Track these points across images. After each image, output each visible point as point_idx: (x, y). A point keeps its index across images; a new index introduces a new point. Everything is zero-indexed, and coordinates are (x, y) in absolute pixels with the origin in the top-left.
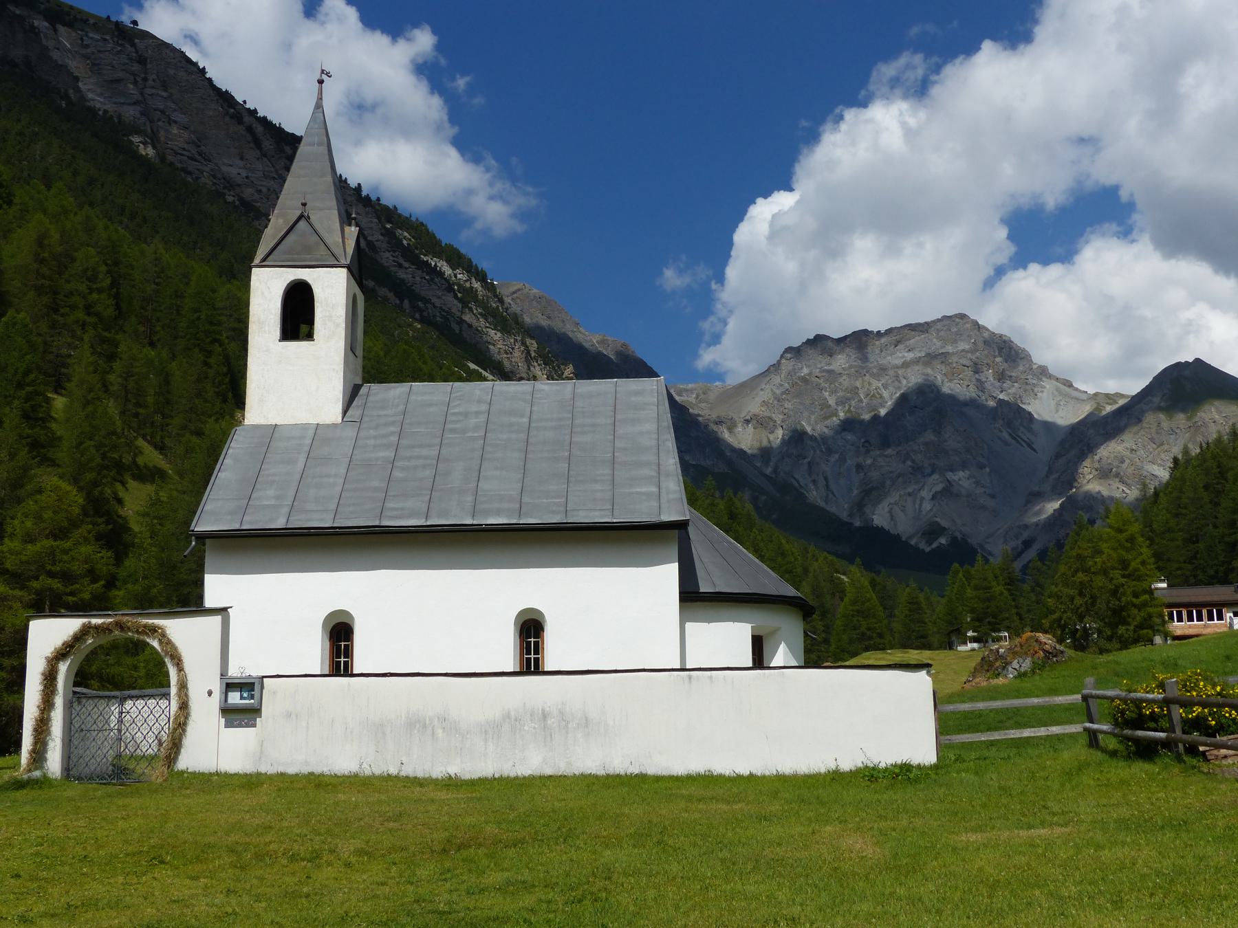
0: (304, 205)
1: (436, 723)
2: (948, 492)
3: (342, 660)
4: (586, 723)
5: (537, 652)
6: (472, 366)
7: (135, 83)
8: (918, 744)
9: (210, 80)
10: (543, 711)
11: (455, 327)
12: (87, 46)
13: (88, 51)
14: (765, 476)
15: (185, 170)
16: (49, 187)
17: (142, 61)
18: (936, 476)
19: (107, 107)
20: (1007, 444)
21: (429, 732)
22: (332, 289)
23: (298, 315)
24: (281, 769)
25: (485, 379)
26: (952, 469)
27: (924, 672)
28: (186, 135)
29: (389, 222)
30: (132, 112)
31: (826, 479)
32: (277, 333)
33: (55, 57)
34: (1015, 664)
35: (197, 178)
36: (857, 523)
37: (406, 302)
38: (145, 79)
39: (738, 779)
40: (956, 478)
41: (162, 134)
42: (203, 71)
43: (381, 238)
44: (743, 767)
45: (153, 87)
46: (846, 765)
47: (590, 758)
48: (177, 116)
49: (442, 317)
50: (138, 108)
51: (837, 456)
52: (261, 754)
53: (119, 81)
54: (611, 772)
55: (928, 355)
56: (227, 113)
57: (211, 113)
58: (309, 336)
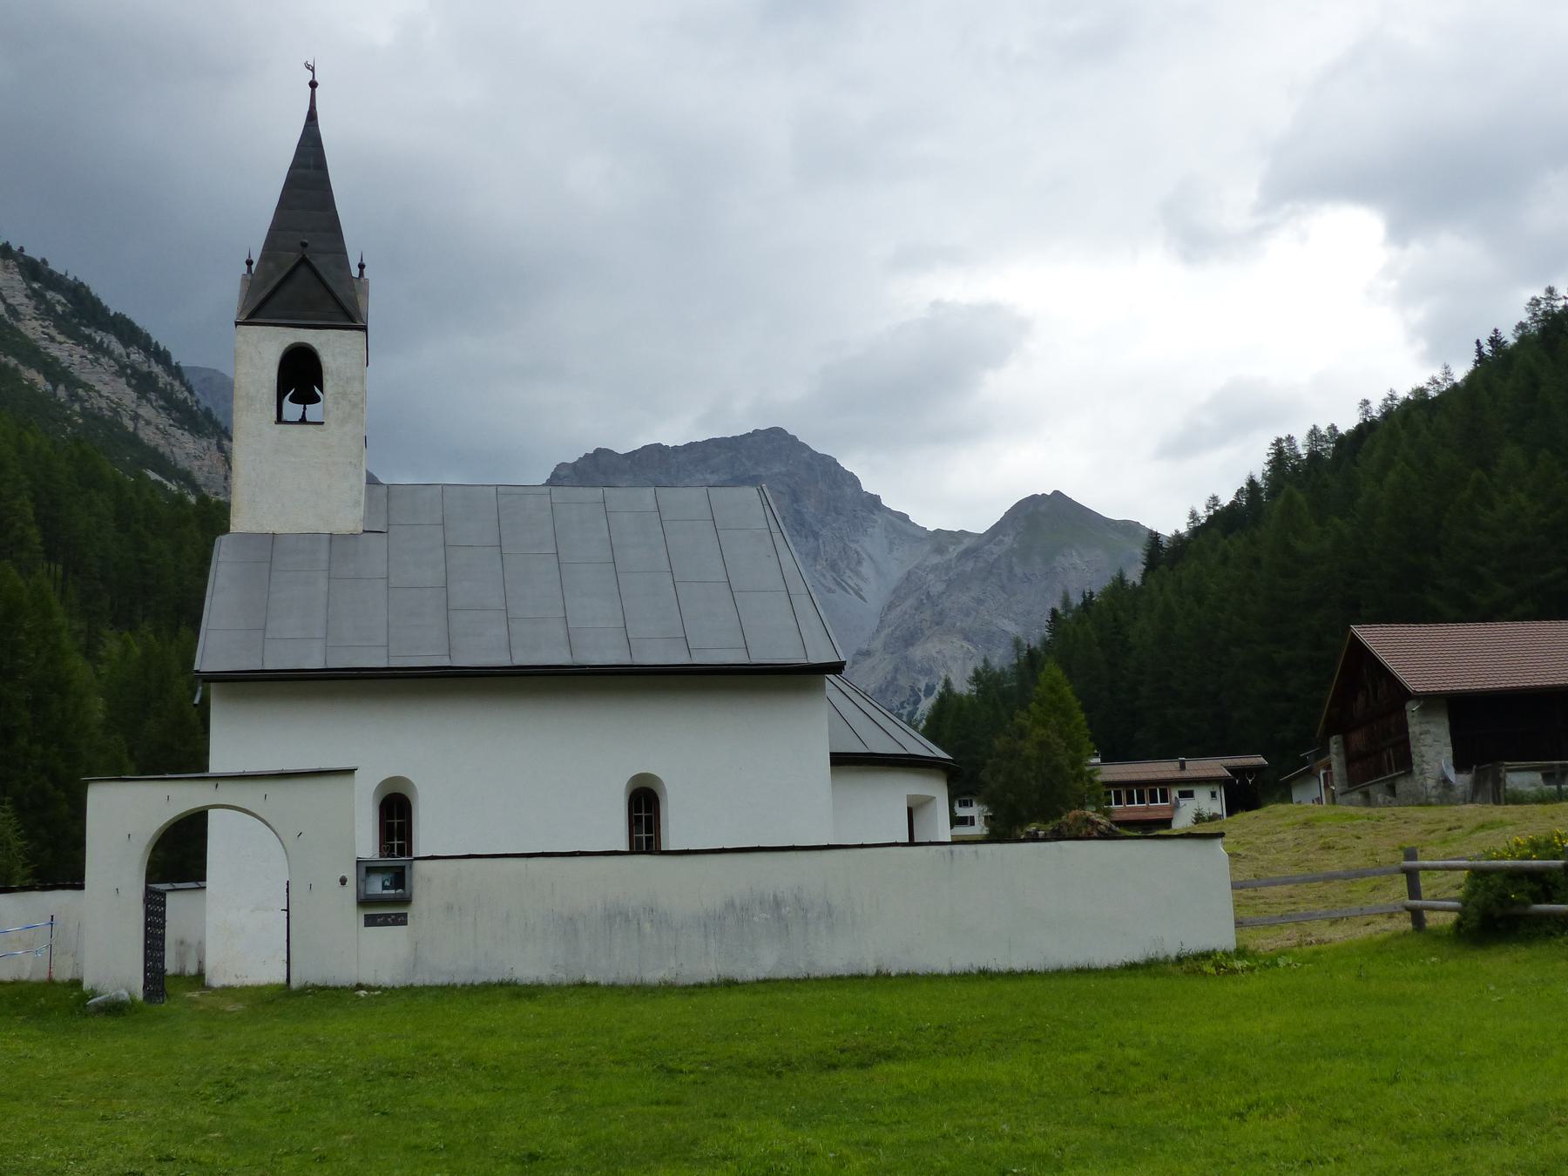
11: (130, 426)
20: (830, 591)
29: (36, 279)
37: (61, 388)
43: (26, 301)
47: (836, 955)
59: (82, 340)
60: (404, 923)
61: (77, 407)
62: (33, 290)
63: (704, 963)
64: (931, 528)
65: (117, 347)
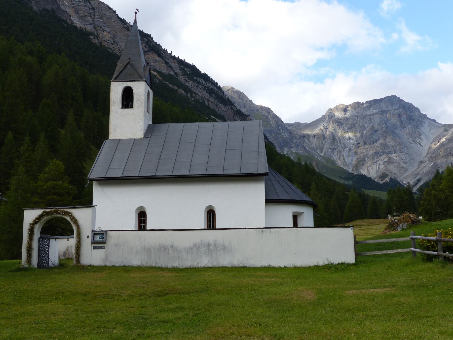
0: (130, 58)
1: (169, 248)
2: (390, 162)
3: (143, 224)
4: (224, 248)
5: (213, 222)
6: (213, 117)
7: (91, 16)
8: (348, 256)
9: (117, 15)
10: (208, 243)
11: (206, 103)
12: (74, 4)
13: (74, 5)
14: (321, 156)
15: (109, 48)
16: (60, 55)
17: (93, 9)
18: (384, 156)
19: (81, 26)
20: (411, 143)
21: (167, 251)
22: (140, 89)
23: (128, 99)
24: (114, 264)
25: (217, 121)
26: (390, 153)
27: (351, 228)
28: (109, 35)
29: (182, 65)
30: (90, 28)
31: (343, 157)
32: (120, 105)
33: (62, 8)
34: (401, 225)
35: (113, 51)
36: (355, 174)
38: (94, 15)
39: (280, 268)
40: (392, 156)
41: (101, 35)
42: (115, 12)
44: (282, 264)
45: (97, 18)
46: (321, 263)
47: (226, 261)
48: (106, 28)
49: (202, 99)
50: (92, 26)
51: (347, 149)
52: (106, 259)
53: (85, 16)
54: (233, 266)
55: (381, 111)
56: (124, 27)
57: (118, 27)
58: (132, 107)
59: (194, 81)
60: (104, 249)
61: (193, 99)
62: (181, 68)
63: (188, 262)
64: (443, 123)
65: (204, 82)
